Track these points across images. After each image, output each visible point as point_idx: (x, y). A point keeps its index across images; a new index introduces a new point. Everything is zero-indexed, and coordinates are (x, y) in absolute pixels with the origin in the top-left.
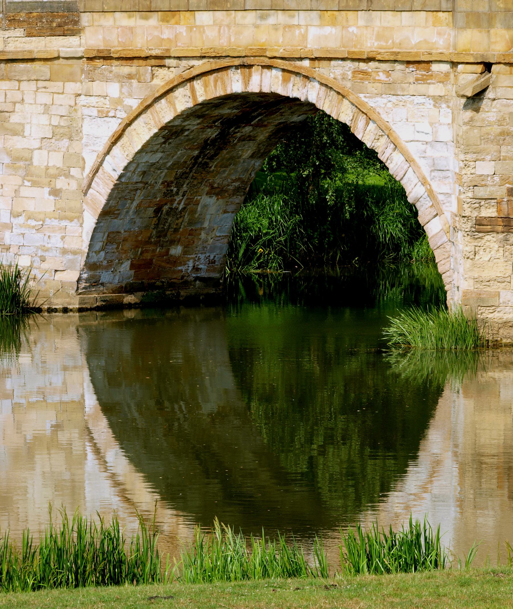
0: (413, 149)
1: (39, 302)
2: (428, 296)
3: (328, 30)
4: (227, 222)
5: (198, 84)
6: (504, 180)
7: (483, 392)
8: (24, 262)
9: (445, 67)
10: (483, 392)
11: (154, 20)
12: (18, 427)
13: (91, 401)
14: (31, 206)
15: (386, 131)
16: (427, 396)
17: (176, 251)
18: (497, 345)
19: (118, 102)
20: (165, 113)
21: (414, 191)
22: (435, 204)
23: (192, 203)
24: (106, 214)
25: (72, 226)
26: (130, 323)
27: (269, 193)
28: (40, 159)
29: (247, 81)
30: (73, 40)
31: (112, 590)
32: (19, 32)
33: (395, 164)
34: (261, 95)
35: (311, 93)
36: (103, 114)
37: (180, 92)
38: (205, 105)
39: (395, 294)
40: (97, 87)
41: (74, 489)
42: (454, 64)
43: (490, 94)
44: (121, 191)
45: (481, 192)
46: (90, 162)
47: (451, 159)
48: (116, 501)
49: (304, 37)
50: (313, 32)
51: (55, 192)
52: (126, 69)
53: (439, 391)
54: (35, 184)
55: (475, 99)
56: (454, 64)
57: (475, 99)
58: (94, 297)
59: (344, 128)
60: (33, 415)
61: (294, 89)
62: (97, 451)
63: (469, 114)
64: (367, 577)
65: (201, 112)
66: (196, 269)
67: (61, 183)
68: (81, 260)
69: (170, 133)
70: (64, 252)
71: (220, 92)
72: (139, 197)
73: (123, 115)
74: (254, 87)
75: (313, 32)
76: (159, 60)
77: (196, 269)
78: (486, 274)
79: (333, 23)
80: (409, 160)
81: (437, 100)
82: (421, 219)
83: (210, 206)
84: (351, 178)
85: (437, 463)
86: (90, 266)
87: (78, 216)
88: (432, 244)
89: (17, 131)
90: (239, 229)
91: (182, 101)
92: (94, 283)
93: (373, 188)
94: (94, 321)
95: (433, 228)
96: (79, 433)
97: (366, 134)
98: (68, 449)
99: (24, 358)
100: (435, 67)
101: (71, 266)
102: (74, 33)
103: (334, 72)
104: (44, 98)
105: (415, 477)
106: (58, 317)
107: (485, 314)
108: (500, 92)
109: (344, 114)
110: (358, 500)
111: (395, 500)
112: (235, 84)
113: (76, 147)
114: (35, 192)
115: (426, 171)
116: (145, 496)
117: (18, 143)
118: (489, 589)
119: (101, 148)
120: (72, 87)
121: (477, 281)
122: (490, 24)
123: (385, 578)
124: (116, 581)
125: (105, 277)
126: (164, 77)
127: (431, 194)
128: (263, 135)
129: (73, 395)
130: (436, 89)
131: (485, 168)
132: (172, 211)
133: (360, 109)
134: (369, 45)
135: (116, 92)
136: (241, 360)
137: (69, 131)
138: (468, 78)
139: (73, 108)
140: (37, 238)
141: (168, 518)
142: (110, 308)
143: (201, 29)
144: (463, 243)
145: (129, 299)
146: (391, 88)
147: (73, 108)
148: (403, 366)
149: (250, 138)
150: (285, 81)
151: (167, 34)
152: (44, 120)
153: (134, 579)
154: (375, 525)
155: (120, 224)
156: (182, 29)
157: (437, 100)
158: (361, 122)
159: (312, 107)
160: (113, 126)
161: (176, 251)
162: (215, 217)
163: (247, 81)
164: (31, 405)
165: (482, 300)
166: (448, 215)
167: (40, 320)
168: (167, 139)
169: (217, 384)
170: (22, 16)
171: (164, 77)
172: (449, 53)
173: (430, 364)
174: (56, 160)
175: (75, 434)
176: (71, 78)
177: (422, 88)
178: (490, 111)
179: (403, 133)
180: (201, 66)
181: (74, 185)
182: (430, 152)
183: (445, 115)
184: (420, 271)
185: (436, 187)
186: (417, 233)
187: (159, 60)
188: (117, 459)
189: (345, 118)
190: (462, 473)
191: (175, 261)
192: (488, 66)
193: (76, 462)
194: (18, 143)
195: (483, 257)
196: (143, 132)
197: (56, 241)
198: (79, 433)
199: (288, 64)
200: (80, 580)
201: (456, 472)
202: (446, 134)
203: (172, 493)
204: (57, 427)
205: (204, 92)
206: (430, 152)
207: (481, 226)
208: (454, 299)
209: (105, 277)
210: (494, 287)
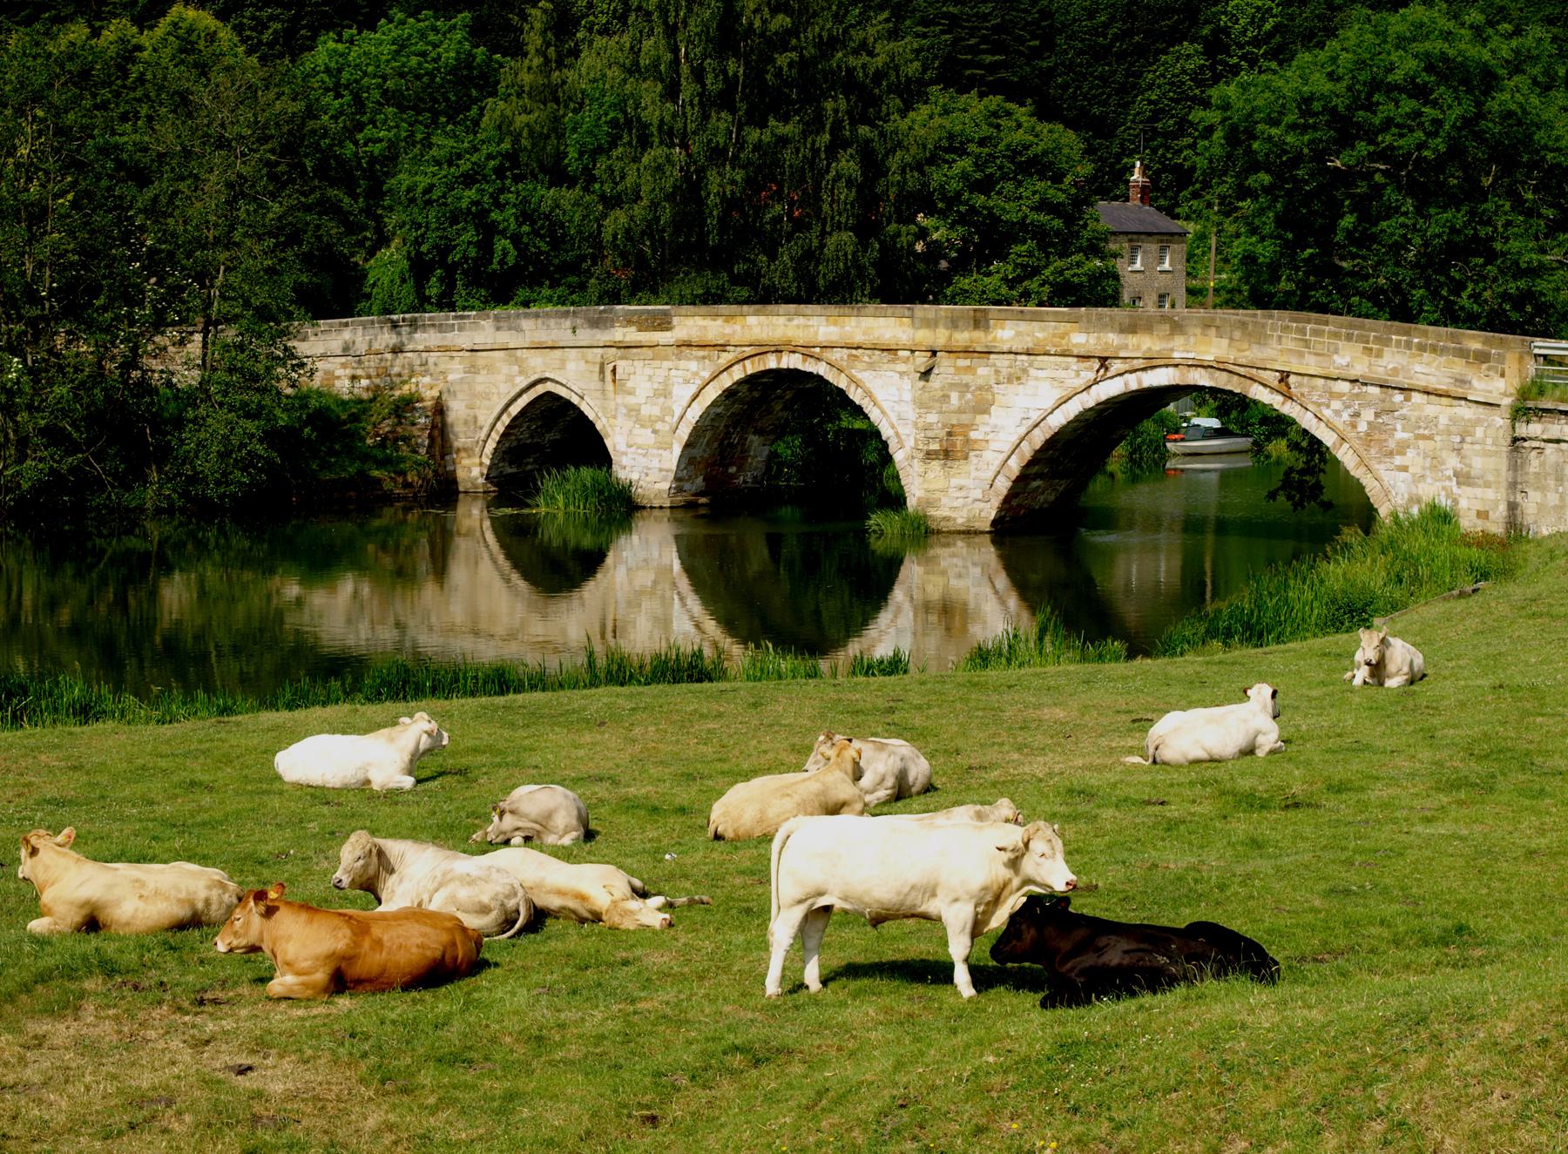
0: (885, 405)
1: (645, 502)
2: (895, 500)
3: (832, 329)
4: (766, 451)
5: (747, 363)
6: (944, 426)
7: (929, 562)
8: (635, 477)
9: (907, 353)
10: (929, 562)
11: (720, 322)
12: (631, 582)
13: (677, 565)
14: (640, 441)
15: (868, 394)
16: (892, 566)
17: (733, 470)
18: (939, 532)
19: (696, 374)
20: (727, 381)
21: (886, 432)
22: (900, 441)
23: (743, 439)
24: (688, 445)
25: (665, 454)
26: (703, 516)
27: (792, 433)
28: (646, 411)
29: (779, 361)
30: (668, 334)
31: (697, 686)
32: (633, 329)
33: (874, 415)
34: (788, 370)
35: (820, 369)
36: (687, 382)
37: (736, 367)
38: (752, 376)
39: (873, 499)
40: (683, 364)
41: (664, 622)
42: (913, 351)
43: (935, 371)
44: (697, 432)
45: (930, 434)
46: (678, 412)
47: (910, 413)
48: (693, 630)
49: (816, 333)
50: (822, 330)
51: (655, 432)
52: (701, 353)
53: (901, 562)
54: (642, 426)
55: (926, 374)
56: (913, 351)
57: (926, 374)
58: (680, 499)
59: (841, 392)
60: (640, 573)
61: (810, 367)
62: (682, 599)
63: (922, 383)
64: (861, 679)
65: (751, 380)
66: (745, 482)
67: (659, 426)
68: (672, 476)
69: (729, 394)
70: (661, 470)
71: (762, 368)
72: (709, 435)
73: (699, 382)
74: (784, 365)
75: (822, 330)
76: (723, 347)
77: (745, 482)
78: (932, 487)
79: (835, 324)
80: (883, 412)
81: (902, 374)
82: (891, 451)
83: (754, 440)
84: (844, 424)
85: (899, 610)
86: (677, 479)
87: (670, 447)
88: (898, 466)
89: (631, 393)
90: (774, 455)
91: (738, 374)
92: (679, 490)
93: (859, 431)
94: (680, 514)
95: (899, 457)
96: (577, 467)
97: (856, 396)
98: (663, 597)
99: (635, 538)
100: (900, 353)
101: (664, 479)
102: (668, 330)
103: (837, 355)
104: (648, 371)
105: (884, 617)
106: (656, 513)
107: (932, 512)
108: (942, 370)
109: (842, 382)
110: (848, 631)
111: (872, 632)
112: (772, 363)
113: (669, 403)
114: (642, 431)
115: (894, 420)
116: (711, 626)
117: (631, 400)
118: (938, 687)
119: (685, 404)
120: (666, 364)
121: (928, 491)
122: (936, 326)
123: (872, 679)
124: (700, 680)
125: (687, 486)
126: (725, 358)
127: (897, 434)
128: (789, 395)
129: (666, 561)
130: (901, 367)
131: (932, 418)
132: (731, 445)
133: (852, 380)
134: (858, 338)
135: (695, 368)
136: (774, 542)
137: (664, 392)
138: (922, 360)
139: (667, 377)
140: (644, 461)
141: (727, 643)
142: (690, 506)
143: (750, 327)
144: (918, 466)
145: (703, 500)
146: (871, 366)
147: (667, 377)
148: (878, 545)
149: (780, 397)
150: (804, 361)
151: (728, 330)
152: (648, 385)
153: (711, 680)
154: (1344, 387)
155: (696, 452)
156: (738, 328)
157: (902, 374)
158: (853, 387)
159: (820, 378)
160: (693, 389)
161: (733, 470)
162: (758, 448)
163: (779, 361)
164: (638, 569)
165: (929, 503)
166: (908, 448)
167: (645, 513)
168: (727, 397)
169: (758, 556)
170: (635, 318)
171: (725, 358)
172: (909, 344)
173: (896, 543)
174: (656, 411)
175: (667, 586)
176: (666, 358)
177: (892, 366)
178: (936, 381)
179: (879, 395)
180: (749, 351)
181: (667, 428)
182: (897, 408)
183: (906, 384)
184: (891, 484)
185: (901, 431)
186: (887, 459)
187: (723, 347)
188: (694, 604)
189: (842, 385)
190: (915, 616)
191: (734, 476)
192: (934, 353)
193: (666, 604)
194: (631, 400)
195: (931, 475)
196: (712, 393)
197: (655, 464)
198: (577, 467)
199: (806, 350)
200: (676, 681)
201: (911, 614)
202: (908, 396)
203: (729, 625)
204: (655, 583)
205: (751, 368)
206: (897, 408)
207: (930, 456)
208: (911, 503)
209: (687, 486)
210: (938, 495)
